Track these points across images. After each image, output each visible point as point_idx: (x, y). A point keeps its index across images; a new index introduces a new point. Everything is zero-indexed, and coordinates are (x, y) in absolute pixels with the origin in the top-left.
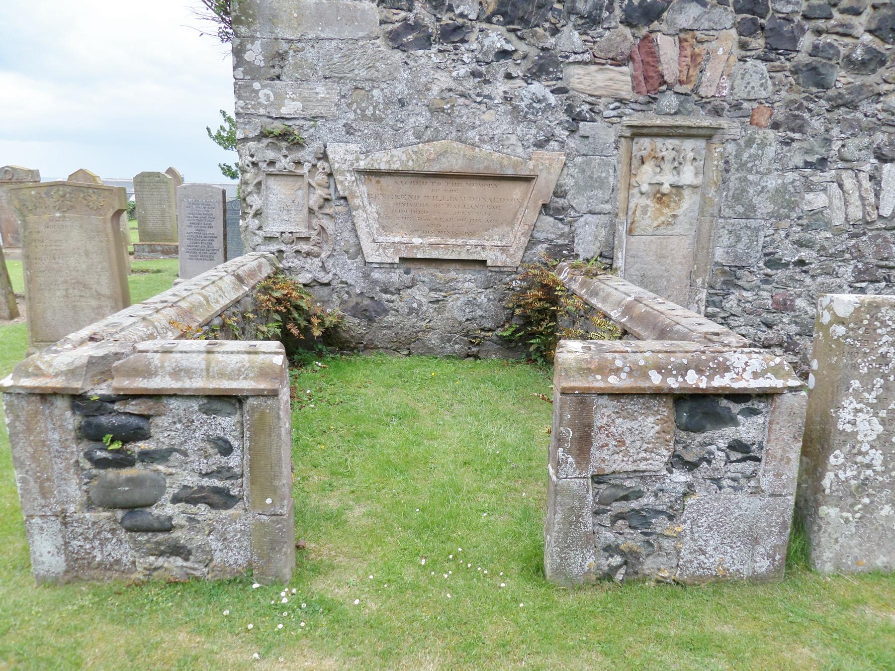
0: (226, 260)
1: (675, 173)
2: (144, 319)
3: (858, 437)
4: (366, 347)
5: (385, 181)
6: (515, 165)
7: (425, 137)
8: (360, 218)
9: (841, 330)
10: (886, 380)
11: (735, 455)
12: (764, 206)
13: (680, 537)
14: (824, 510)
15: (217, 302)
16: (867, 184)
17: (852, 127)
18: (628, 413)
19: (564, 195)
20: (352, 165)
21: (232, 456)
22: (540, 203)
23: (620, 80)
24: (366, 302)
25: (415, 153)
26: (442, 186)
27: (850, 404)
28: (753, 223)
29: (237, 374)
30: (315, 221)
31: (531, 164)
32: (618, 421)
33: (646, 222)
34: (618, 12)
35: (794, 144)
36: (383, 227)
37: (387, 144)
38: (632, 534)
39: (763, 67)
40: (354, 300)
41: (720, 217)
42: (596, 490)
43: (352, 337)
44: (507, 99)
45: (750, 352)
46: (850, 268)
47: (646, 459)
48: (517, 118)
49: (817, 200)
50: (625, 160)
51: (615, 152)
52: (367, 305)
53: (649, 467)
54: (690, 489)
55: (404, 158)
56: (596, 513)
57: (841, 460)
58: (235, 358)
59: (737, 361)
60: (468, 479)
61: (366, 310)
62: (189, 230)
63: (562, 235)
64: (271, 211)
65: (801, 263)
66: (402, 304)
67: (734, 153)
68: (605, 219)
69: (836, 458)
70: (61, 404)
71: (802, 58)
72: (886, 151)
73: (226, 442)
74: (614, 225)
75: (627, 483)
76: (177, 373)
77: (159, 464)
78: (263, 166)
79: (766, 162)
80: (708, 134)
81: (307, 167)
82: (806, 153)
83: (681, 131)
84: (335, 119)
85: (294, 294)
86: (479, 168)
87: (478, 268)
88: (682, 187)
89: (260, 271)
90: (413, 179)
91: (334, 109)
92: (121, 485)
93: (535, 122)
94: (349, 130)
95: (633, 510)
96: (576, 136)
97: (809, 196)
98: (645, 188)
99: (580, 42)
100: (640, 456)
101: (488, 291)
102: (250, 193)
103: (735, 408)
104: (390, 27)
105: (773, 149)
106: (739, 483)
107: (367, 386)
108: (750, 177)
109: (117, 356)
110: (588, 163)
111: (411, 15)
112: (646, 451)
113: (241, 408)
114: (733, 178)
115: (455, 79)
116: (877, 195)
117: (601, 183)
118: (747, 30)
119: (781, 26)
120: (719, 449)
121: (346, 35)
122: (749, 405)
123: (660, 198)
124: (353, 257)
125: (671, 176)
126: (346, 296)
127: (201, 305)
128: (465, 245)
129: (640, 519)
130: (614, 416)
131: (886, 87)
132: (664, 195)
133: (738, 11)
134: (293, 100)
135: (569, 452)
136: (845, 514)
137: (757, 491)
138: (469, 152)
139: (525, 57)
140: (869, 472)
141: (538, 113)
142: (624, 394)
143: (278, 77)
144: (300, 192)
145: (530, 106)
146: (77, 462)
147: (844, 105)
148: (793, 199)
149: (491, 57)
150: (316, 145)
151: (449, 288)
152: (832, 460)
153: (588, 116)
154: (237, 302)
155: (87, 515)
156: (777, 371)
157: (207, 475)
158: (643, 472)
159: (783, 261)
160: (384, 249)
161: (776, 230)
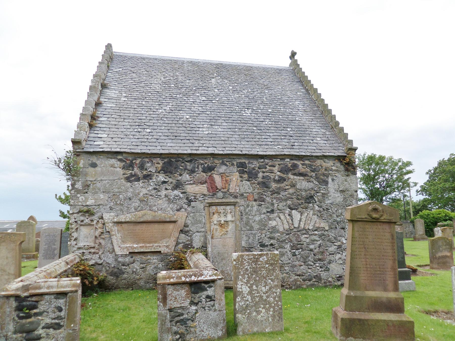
0: (60, 258)
4: (115, 288)
5: (123, 225)
6: (170, 218)
8: (114, 238)
10: (248, 276)
11: (208, 300)
12: (256, 226)
13: (195, 327)
15: (59, 271)
16: (288, 217)
17: (279, 199)
19: (188, 226)
23: (203, 189)
24: (116, 270)
25: (134, 215)
26: (144, 226)
27: (240, 283)
28: (253, 232)
29: (66, 286)
30: (97, 241)
31: (175, 217)
33: (217, 234)
34: (200, 169)
35: (263, 206)
36: (123, 242)
37: (125, 213)
39: (248, 183)
40: (111, 269)
43: (110, 284)
44: (166, 196)
46: (289, 245)
47: (183, 303)
49: (273, 223)
50: (208, 214)
53: (185, 305)
54: (197, 312)
55: (131, 217)
56: (171, 321)
57: (240, 300)
58: (66, 282)
60: (143, 325)
62: (45, 247)
63: (188, 240)
64: (81, 238)
65: (272, 245)
66: (130, 270)
68: (202, 234)
70: (12, 299)
71: (260, 180)
72: (292, 206)
73: (61, 308)
75: (179, 311)
76: (48, 287)
78: (79, 222)
79: (254, 212)
80: (234, 204)
81: (95, 222)
84: (106, 205)
85: (87, 268)
86: (157, 219)
87: (158, 254)
89: (75, 260)
92: (27, 324)
94: (111, 209)
97: (270, 222)
98: (215, 222)
99: (189, 178)
102: (73, 232)
103: (206, 286)
104: (126, 176)
105: (256, 207)
107: (114, 301)
108: (250, 217)
109: (30, 284)
110: (195, 215)
111: (133, 172)
112: (183, 300)
113: (66, 297)
114: (244, 218)
115: (148, 191)
116: (292, 220)
117: (200, 222)
118: (242, 172)
119: (252, 171)
121: (111, 178)
122: (210, 284)
127: (54, 272)
128: (153, 246)
129: (183, 322)
131: (287, 187)
133: (238, 167)
134: (92, 199)
135: (160, 302)
136: (243, 316)
137: (215, 310)
138: (153, 214)
139: (171, 183)
140: (248, 302)
143: (87, 193)
145: (174, 198)
146: (14, 318)
147: (276, 193)
149: (160, 183)
150: (99, 214)
151: (148, 263)
152: (237, 300)
154: (66, 271)
155: (14, 336)
156: (216, 275)
157: (54, 319)
161: (261, 234)
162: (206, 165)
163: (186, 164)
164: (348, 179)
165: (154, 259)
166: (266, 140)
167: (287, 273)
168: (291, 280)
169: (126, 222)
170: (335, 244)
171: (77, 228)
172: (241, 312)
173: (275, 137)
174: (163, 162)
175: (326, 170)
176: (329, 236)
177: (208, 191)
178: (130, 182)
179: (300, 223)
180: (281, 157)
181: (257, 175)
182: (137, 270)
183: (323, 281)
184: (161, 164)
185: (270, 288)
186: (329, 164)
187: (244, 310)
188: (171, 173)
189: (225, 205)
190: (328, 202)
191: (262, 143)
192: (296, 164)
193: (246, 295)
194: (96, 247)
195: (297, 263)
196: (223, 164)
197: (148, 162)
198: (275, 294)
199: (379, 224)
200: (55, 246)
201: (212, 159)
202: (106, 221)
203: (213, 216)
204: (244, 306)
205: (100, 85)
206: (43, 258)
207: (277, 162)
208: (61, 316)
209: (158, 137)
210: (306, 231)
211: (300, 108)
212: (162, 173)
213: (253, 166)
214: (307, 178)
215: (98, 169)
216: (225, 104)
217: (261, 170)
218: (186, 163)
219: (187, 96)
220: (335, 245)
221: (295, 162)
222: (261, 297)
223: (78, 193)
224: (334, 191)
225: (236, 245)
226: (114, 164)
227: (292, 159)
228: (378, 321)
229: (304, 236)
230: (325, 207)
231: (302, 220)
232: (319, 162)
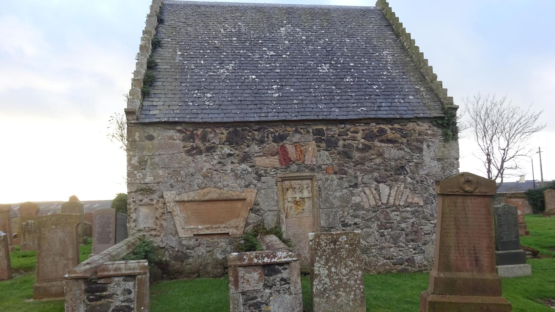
0: (115, 244)
7: (202, 187)
9: (311, 243)
11: (283, 283)
16: (374, 192)
17: (364, 171)
19: (258, 205)
24: (180, 254)
26: (210, 204)
27: (317, 265)
29: (134, 269)
31: (243, 194)
33: (292, 212)
34: (271, 138)
39: (327, 153)
40: (175, 253)
44: (232, 171)
46: (376, 225)
50: (281, 189)
64: (140, 220)
65: (355, 224)
71: (340, 149)
73: (130, 290)
76: (115, 270)
78: (137, 202)
81: (155, 201)
87: (226, 236)
91: (166, 178)
97: (354, 198)
98: (290, 199)
103: (280, 268)
104: (187, 149)
105: (336, 181)
116: (379, 196)
118: (318, 141)
121: (170, 152)
123: (296, 203)
124: (174, 236)
126: (171, 252)
131: (373, 157)
133: (314, 135)
137: (291, 294)
139: (238, 156)
140: (326, 286)
144: (152, 211)
145: (241, 173)
149: (225, 156)
152: (314, 283)
156: (290, 256)
157: (124, 301)
161: (344, 212)
162: (277, 134)
163: (254, 134)
164: (447, 145)
165: (223, 243)
166: (347, 101)
167: (374, 256)
168: (379, 264)
169: (188, 201)
170: (431, 222)
171: (136, 209)
172: (318, 296)
173: (357, 97)
174: (228, 131)
175: (420, 135)
176: (424, 213)
177: (281, 163)
178: (192, 155)
179: (388, 198)
180: (365, 121)
181: (337, 143)
182: (203, 254)
183: (417, 265)
184: (226, 134)
185: (351, 270)
186: (425, 126)
187: (322, 293)
188: (237, 144)
189: (299, 179)
190: (422, 172)
191: (342, 106)
192: (384, 128)
193: (324, 278)
195: (386, 244)
196: (296, 131)
197: (211, 133)
198: (356, 277)
199: (473, 198)
200: (109, 229)
201: (283, 126)
202: (167, 200)
205: (153, 44)
206: (97, 242)
207: (361, 128)
208: (131, 299)
209: (221, 103)
210: (397, 208)
211: (389, 60)
212: (227, 144)
213: (332, 133)
214: (396, 145)
215: (155, 141)
216: (298, 59)
217: (342, 137)
218: (254, 132)
219: (252, 51)
220: (431, 223)
221: (382, 126)
222: (340, 280)
223: (135, 170)
224: (430, 159)
225: (314, 225)
226: (173, 136)
227: (379, 124)
229: (394, 213)
230: (418, 178)
231: (392, 195)
232: (410, 125)
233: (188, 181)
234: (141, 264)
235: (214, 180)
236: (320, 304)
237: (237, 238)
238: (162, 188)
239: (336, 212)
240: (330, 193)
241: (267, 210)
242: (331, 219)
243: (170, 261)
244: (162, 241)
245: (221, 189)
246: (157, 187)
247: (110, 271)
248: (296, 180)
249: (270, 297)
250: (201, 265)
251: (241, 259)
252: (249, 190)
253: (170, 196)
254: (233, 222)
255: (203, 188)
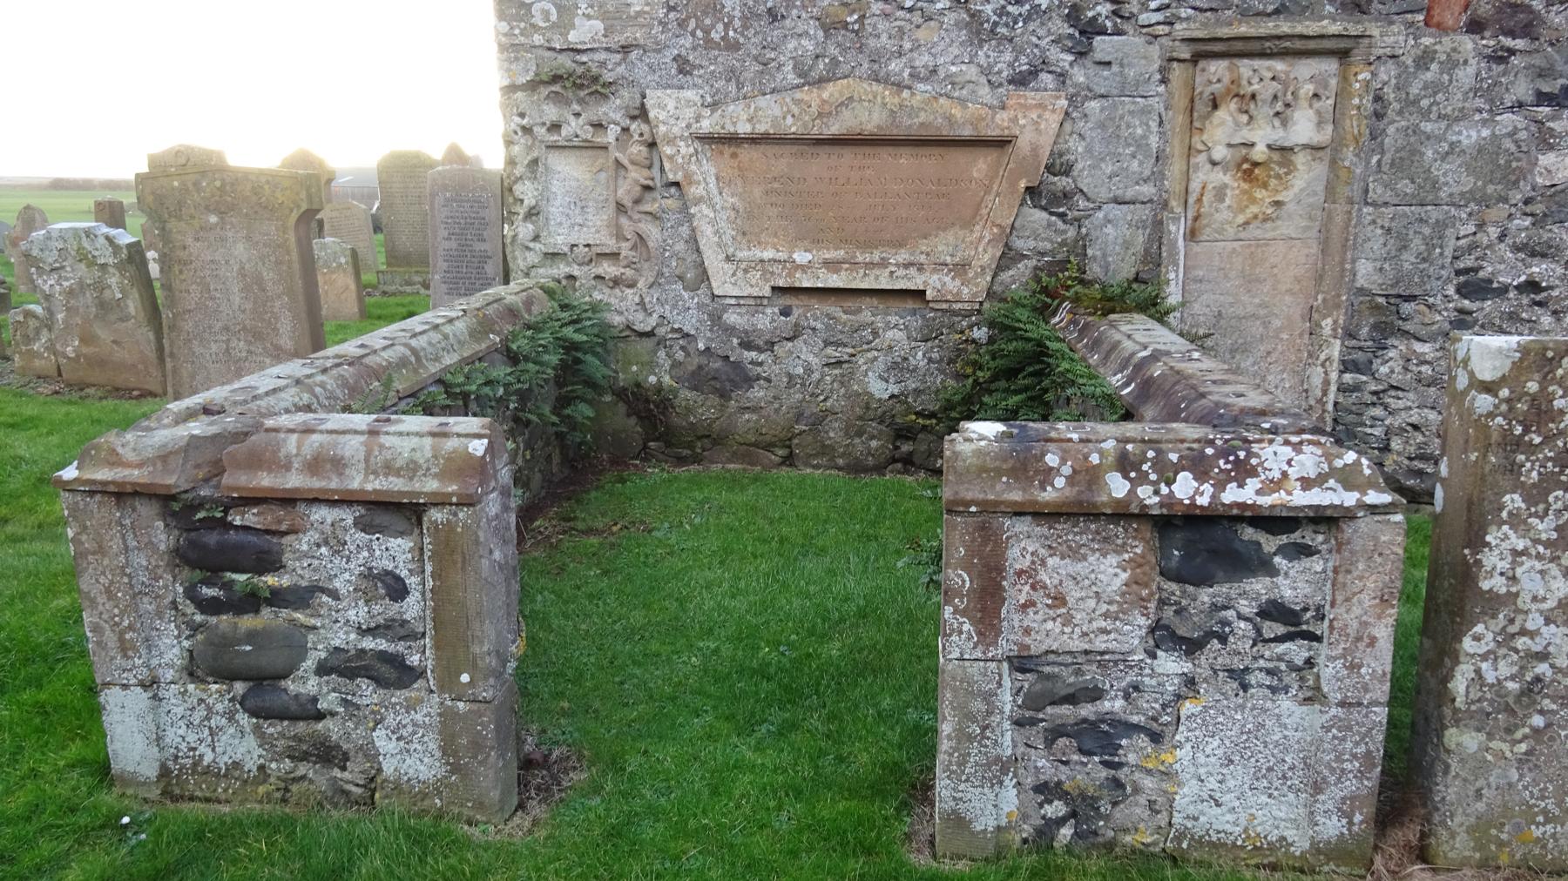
1: (1277, 122)
2: (298, 382)
3: (1519, 602)
5: (747, 153)
6: (976, 121)
7: (814, 74)
8: (702, 212)
9: (1484, 402)
11: (1272, 629)
12: (1454, 178)
14: (1452, 736)
18: (1070, 547)
19: (1067, 171)
20: (689, 126)
21: (411, 600)
22: (1023, 184)
24: (718, 364)
26: (848, 156)
27: (1501, 541)
29: (412, 469)
31: (1002, 118)
32: (1050, 562)
33: (1222, 215)
35: (1514, 60)
36: (744, 234)
38: (1086, 764)
41: (1367, 204)
42: (1018, 685)
45: (1301, 443)
48: (978, 33)
50: (1181, 102)
51: (1161, 89)
52: (717, 370)
53: (1113, 646)
59: (1271, 457)
61: (714, 378)
62: (447, 245)
63: (1063, 243)
64: (555, 210)
65: (1532, 286)
66: (776, 368)
67: (1393, 81)
69: (1476, 641)
73: (399, 579)
74: (1161, 222)
76: (315, 465)
77: (296, 609)
78: (540, 131)
81: (613, 132)
82: (1540, 76)
83: (1288, 44)
86: (911, 125)
88: (1292, 149)
90: (795, 149)
91: (657, 29)
93: (1011, 41)
94: (684, 67)
95: (1085, 720)
96: (1088, 62)
98: (1219, 153)
100: (1095, 625)
101: (929, 344)
103: (1269, 543)
105: (1471, 70)
106: (1280, 680)
112: (1106, 616)
114: (1391, 130)
120: (1240, 617)
122: (1296, 537)
123: (1249, 170)
124: (692, 288)
125: (1269, 129)
126: (680, 355)
129: (1101, 738)
130: (1042, 552)
132: (1256, 164)
134: (589, 17)
135: (964, 613)
137: (1314, 696)
140: (1542, 668)
141: (1016, 23)
142: (1061, 515)
144: (603, 175)
146: (174, 602)
148: (1514, 164)
152: (1468, 644)
153: (1109, 24)
156: (1348, 479)
157: (370, 632)
158: (1102, 653)
159: (1495, 285)
160: (746, 271)
161: (1481, 226)
169: (755, 140)
171: (535, 162)
172: (1481, 720)
182: (809, 370)
193: (1534, 622)
194: (624, 253)
202: (663, 129)
203: (1208, 116)
204: (1512, 686)
208: (404, 623)
225: (1319, 278)
228: (1445, 499)
233: (753, 45)
234: (451, 444)
235: (872, 42)
236: (1482, 767)
237: (955, 313)
238: (641, 71)
239: (1441, 226)
240: (1427, 127)
241: (1104, 194)
242: (1409, 259)
243: (675, 392)
244: (642, 303)
245: (900, 86)
246: (621, 69)
247: (287, 467)
248: (1263, 55)
249: (1179, 697)
250: (799, 417)
251: (1026, 466)
252: (1030, 96)
253: (675, 109)
254: (944, 245)
255: (821, 81)
